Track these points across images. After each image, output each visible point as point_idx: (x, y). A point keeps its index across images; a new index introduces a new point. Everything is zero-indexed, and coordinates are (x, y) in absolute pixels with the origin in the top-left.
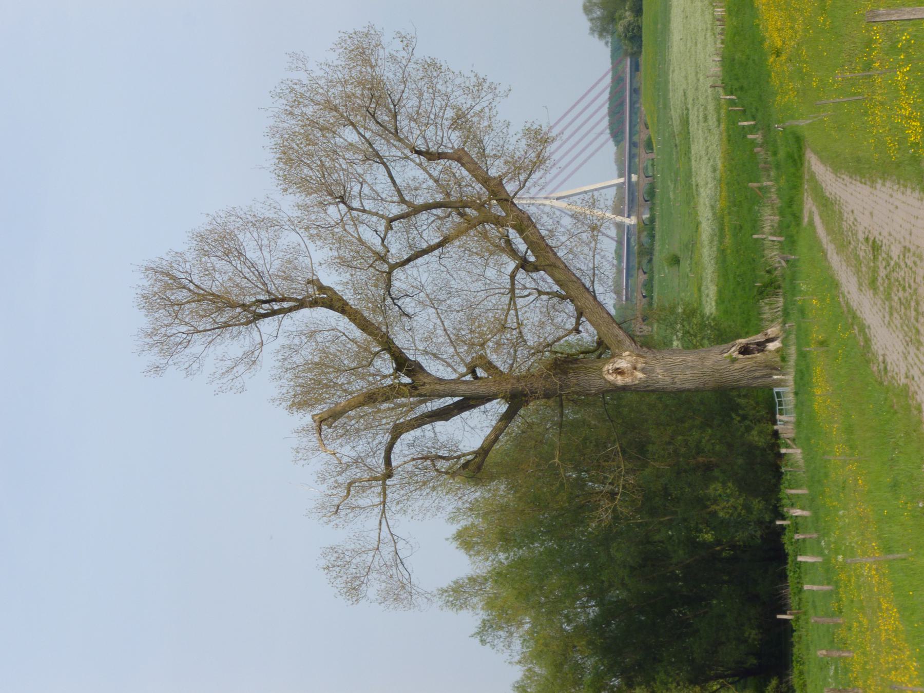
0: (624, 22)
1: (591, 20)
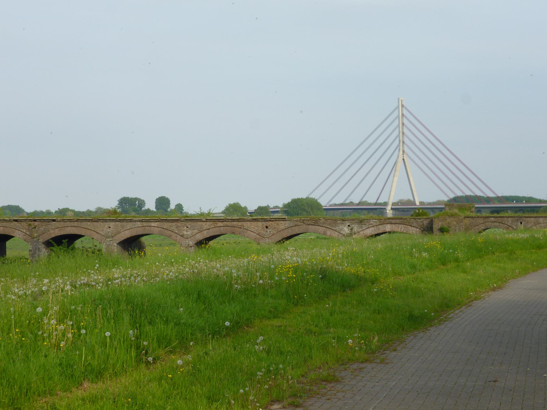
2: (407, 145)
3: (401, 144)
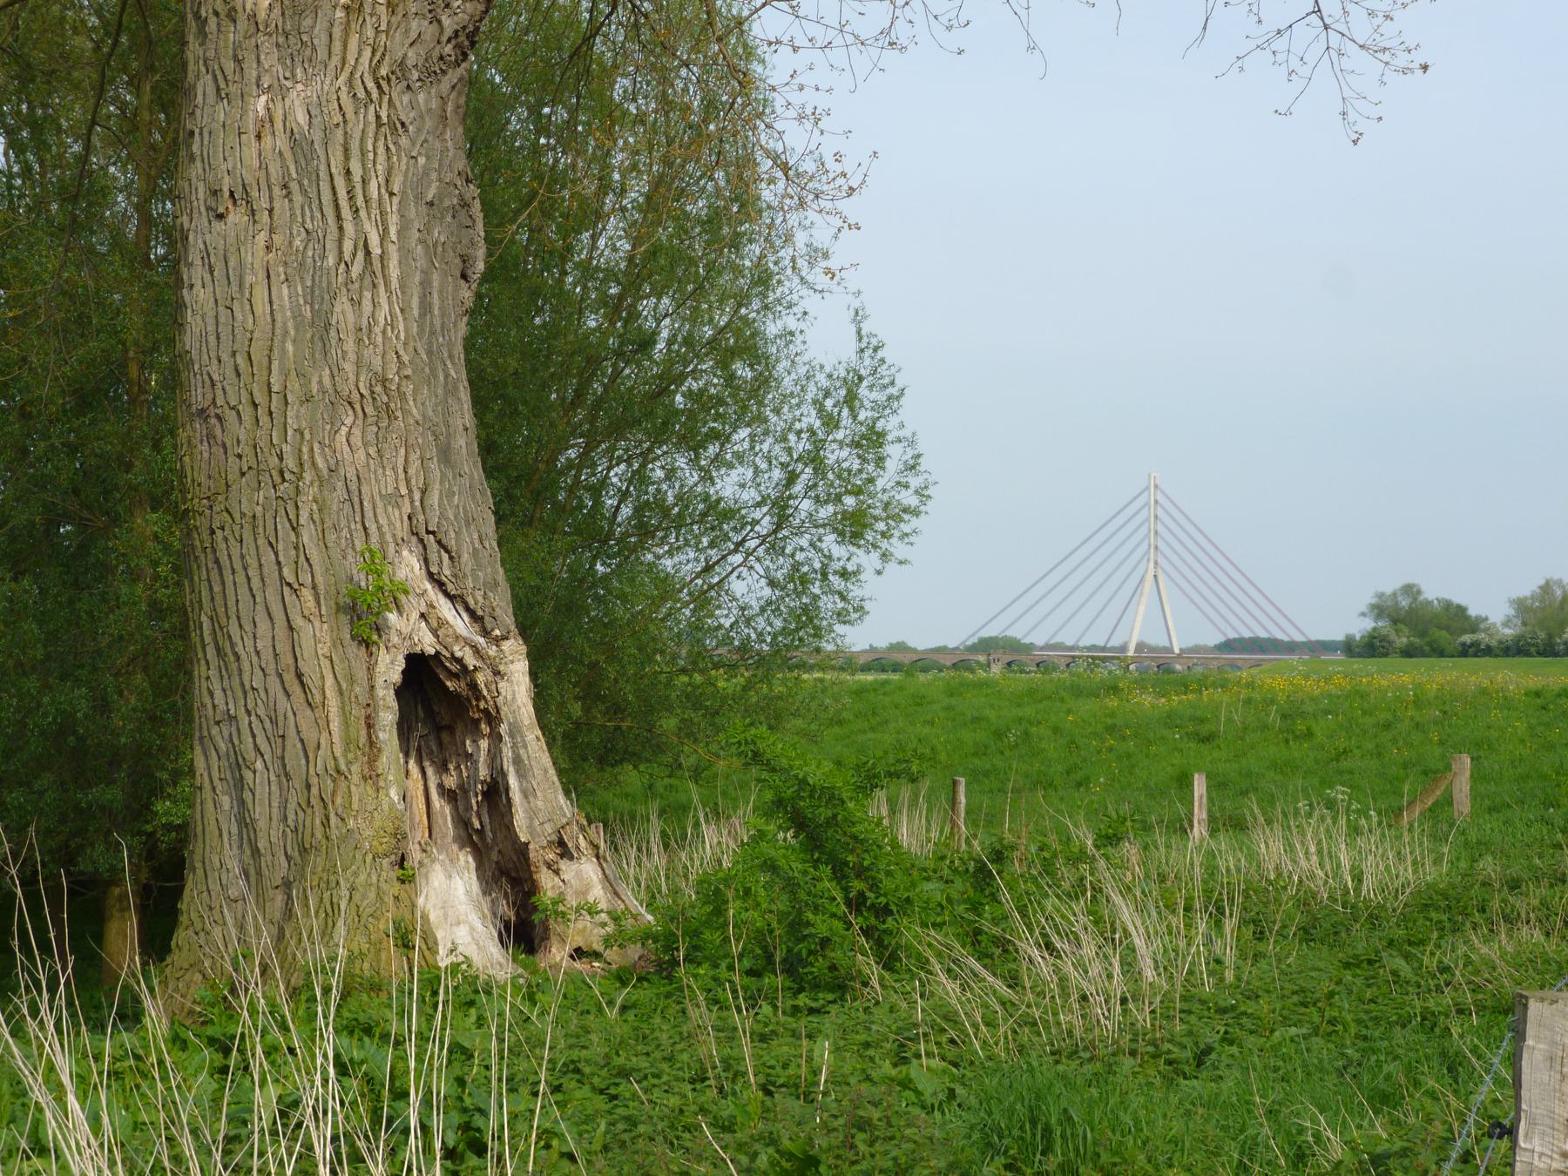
0: (1393, 636)
1: (1395, 594)
2: (1162, 538)
3: (1152, 550)
